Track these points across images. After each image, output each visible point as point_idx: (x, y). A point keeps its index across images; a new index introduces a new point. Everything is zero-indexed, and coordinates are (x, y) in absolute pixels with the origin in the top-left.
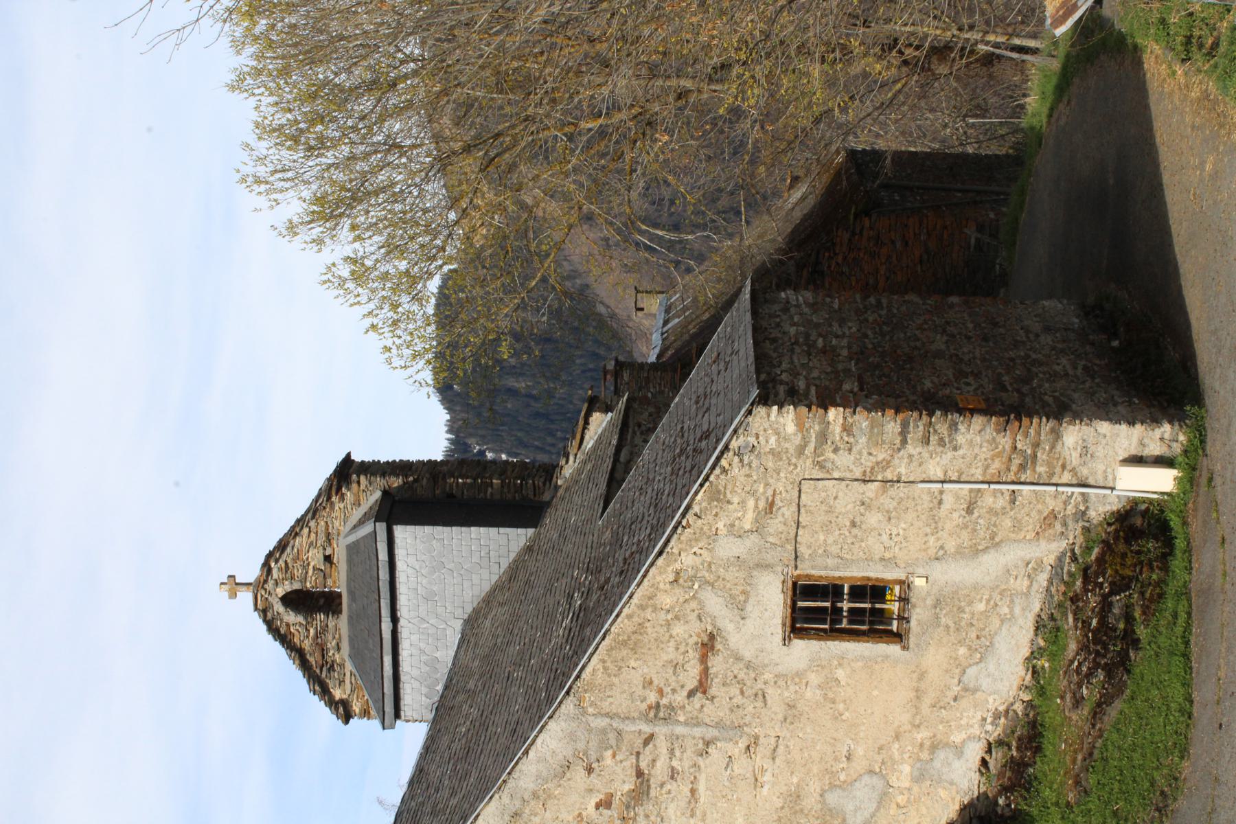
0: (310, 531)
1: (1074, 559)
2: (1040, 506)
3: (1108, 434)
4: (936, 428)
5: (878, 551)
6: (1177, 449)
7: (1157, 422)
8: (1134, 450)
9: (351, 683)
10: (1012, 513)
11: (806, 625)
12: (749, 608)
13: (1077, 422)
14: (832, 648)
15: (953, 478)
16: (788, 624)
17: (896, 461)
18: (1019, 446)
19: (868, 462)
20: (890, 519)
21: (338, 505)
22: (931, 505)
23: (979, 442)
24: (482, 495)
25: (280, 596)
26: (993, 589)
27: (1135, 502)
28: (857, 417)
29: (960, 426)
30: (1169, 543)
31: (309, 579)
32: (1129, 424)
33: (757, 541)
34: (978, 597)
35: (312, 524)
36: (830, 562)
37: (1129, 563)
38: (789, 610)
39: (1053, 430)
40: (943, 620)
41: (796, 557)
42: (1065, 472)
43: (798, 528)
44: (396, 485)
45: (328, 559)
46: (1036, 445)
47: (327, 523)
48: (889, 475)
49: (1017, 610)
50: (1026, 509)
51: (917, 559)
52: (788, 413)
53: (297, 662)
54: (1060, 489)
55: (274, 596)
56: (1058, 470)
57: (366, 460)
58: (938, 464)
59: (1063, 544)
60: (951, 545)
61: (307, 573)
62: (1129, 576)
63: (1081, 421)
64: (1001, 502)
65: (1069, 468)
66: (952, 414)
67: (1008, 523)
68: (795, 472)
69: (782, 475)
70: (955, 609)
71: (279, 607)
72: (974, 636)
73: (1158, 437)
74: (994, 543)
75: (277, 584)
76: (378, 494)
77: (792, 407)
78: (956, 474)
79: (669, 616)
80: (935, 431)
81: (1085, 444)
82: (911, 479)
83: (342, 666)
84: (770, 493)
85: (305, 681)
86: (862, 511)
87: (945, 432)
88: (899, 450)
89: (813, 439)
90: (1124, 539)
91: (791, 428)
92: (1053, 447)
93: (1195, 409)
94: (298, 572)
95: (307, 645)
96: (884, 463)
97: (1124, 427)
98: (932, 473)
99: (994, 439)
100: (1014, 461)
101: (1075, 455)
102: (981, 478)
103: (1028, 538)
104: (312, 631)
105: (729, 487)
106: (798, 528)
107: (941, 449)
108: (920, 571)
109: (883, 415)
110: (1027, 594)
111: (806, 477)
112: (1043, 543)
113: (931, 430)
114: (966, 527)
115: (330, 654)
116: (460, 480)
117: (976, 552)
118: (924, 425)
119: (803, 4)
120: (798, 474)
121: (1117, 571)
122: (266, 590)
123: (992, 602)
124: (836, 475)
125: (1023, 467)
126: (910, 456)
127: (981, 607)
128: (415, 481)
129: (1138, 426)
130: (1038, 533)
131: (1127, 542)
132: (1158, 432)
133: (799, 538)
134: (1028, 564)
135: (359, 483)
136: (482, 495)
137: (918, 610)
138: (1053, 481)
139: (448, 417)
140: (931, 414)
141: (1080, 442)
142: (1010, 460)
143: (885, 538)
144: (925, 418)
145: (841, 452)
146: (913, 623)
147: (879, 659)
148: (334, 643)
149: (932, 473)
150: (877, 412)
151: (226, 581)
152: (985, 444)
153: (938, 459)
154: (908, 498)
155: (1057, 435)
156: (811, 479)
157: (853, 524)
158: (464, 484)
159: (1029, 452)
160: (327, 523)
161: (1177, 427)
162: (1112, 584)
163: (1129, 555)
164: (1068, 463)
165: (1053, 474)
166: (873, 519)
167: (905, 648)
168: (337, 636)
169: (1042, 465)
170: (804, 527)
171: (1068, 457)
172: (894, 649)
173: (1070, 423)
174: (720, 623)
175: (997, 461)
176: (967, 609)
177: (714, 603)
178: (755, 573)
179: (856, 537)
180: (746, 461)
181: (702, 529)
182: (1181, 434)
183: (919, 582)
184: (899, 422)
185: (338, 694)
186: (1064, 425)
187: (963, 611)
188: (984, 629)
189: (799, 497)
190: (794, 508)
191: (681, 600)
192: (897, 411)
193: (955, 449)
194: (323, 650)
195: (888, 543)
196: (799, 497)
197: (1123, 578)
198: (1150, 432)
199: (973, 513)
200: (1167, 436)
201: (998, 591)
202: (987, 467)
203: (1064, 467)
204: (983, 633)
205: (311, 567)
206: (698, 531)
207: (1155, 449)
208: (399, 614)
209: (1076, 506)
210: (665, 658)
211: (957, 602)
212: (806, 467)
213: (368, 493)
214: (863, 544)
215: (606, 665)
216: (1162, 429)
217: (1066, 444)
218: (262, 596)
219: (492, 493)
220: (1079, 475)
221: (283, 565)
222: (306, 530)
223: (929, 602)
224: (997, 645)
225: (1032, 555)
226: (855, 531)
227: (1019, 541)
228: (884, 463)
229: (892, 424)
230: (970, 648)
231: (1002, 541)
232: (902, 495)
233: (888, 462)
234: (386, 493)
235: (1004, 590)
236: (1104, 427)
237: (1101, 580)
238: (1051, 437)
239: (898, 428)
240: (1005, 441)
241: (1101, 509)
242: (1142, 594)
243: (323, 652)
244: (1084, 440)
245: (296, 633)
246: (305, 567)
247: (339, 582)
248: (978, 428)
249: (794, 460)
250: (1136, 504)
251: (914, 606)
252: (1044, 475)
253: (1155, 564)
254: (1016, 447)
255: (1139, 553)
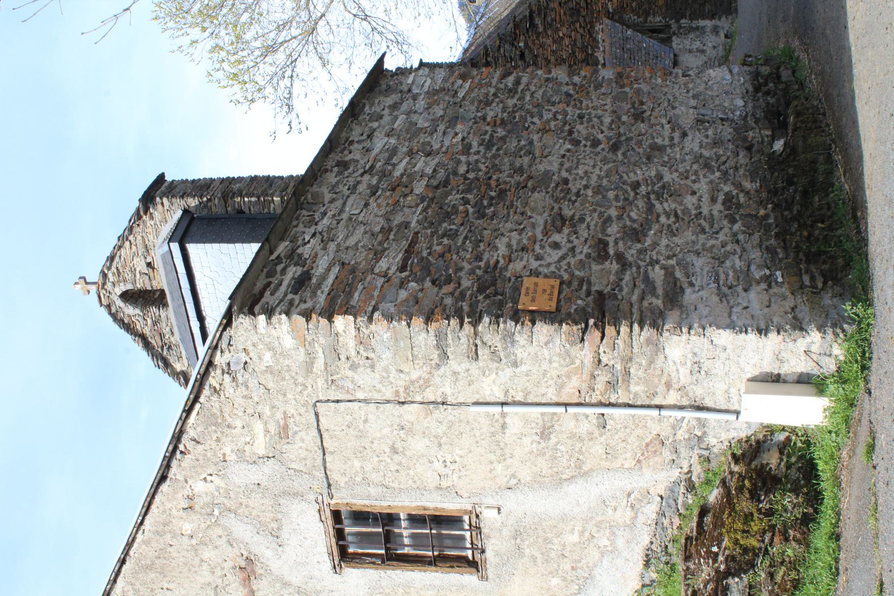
0: (131, 244)
1: (691, 487)
2: (639, 431)
3: (729, 346)
4: (485, 340)
5: (432, 480)
6: (830, 366)
7: (801, 329)
8: (769, 366)
10: (603, 439)
11: (360, 551)
12: (285, 534)
13: (685, 330)
14: (394, 576)
15: (517, 399)
16: (336, 553)
17: (437, 380)
18: (604, 360)
19: (401, 382)
20: (440, 445)
21: (149, 223)
22: (492, 430)
23: (548, 357)
24: (266, 210)
25: (119, 294)
26: (586, 521)
27: (771, 430)
28: (373, 327)
29: (517, 337)
30: (815, 498)
31: (138, 281)
32: (760, 331)
33: (277, 467)
34: (569, 528)
35: (131, 238)
36: (373, 491)
37: (755, 528)
38: (334, 540)
39: (649, 341)
40: (527, 551)
41: (329, 485)
42: (671, 392)
43: (324, 454)
44: (193, 204)
45: (149, 265)
46: (628, 359)
47: (143, 237)
48: (430, 396)
49: (620, 542)
50: (621, 435)
51: (484, 488)
52: (280, 323)
53: (141, 344)
54: (664, 413)
55: (113, 294)
56: (661, 388)
58: (494, 382)
59: (675, 474)
60: (525, 474)
62: (754, 549)
63: (690, 328)
64: (585, 427)
65: (676, 386)
66: (505, 322)
67: (599, 449)
68: (305, 393)
69: (289, 396)
70: (540, 540)
71: (119, 303)
72: (568, 567)
73: (803, 349)
74: (581, 473)
75: (114, 285)
76: (179, 213)
77: (284, 316)
78: (521, 394)
79: (194, 542)
80: (484, 344)
81: (696, 359)
82: (461, 400)
83: (177, 346)
84: (279, 416)
85: (150, 358)
86: (403, 436)
87: (499, 345)
88: (438, 366)
89: (321, 354)
90: (750, 492)
91: (288, 342)
92: (651, 362)
93: (859, 309)
94: (129, 276)
95: (147, 331)
96: (421, 382)
97: (752, 337)
98: (488, 392)
99: (568, 353)
100: (598, 379)
101: (684, 372)
102: (555, 399)
103: (626, 466)
104: (149, 321)
105: (227, 410)
106: (324, 454)
107: (496, 365)
108: (490, 501)
109: (409, 325)
110: (632, 526)
111: (321, 398)
112: (647, 473)
113: (478, 342)
114: (541, 454)
115: (167, 337)
116: (246, 199)
117: (559, 482)
118: (468, 336)
120: (309, 395)
121: (736, 542)
122: (106, 290)
123: (587, 534)
124: (360, 395)
125: (612, 385)
126: (455, 373)
127: (574, 538)
128: (209, 200)
129: (773, 336)
130: (639, 461)
131: (754, 496)
132: (802, 343)
133: (328, 465)
134: (629, 495)
135: (162, 203)
136: (266, 210)
137: (493, 541)
138: (657, 401)
140: (475, 324)
141: (690, 356)
142: (593, 377)
143: (438, 466)
144: (468, 328)
145: (361, 369)
146: (489, 554)
147: (454, 589)
148: (168, 329)
149: (488, 392)
150: (400, 319)
151: (78, 281)
152: (556, 358)
153: (493, 376)
154: (460, 421)
155: (658, 348)
156: (328, 401)
157: (394, 450)
158: (250, 202)
159: (618, 367)
160: (143, 237)
161: (830, 336)
162: (730, 559)
163: (756, 515)
164: (675, 381)
165: (655, 394)
166: (418, 445)
167: (483, 578)
168: (169, 324)
169: (637, 384)
170: (332, 453)
171: (673, 374)
172: (469, 579)
173: (672, 332)
174: (255, 549)
175: (574, 378)
176: (555, 541)
177: (243, 531)
178: (282, 501)
179: (400, 464)
180: (240, 380)
181: (205, 455)
182: (835, 346)
183: (488, 515)
184: (432, 332)
185: (178, 367)
186: (666, 334)
187: (551, 542)
188: (580, 562)
189: (318, 421)
190: (315, 433)
191: (203, 526)
192: (428, 320)
193: (515, 364)
194: (161, 334)
195: (443, 471)
196: (318, 421)
197: (745, 550)
198: (791, 344)
199: (549, 439)
200: (815, 348)
201: (594, 522)
202: (562, 386)
203: (668, 385)
204: (579, 565)
205: (137, 272)
206: (201, 458)
207: (797, 365)
208: (204, 314)
209: (689, 431)
210: (202, 581)
211: (541, 533)
212: (320, 388)
213: (172, 212)
214: (411, 472)
215: (135, 587)
216: (808, 339)
217: (670, 358)
218: (104, 295)
219: (274, 208)
220: (691, 394)
221: (115, 271)
222: (127, 243)
223: (506, 532)
224: (598, 577)
225: (635, 485)
226: (397, 458)
227: (616, 470)
228: (421, 382)
229: (424, 334)
230: (564, 579)
231: (592, 470)
232: (451, 418)
233: (427, 381)
234: (186, 212)
235: (601, 522)
236: (724, 337)
237: (715, 549)
238: (648, 350)
239: (432, 341)
240: (585, 354)
241: (725, 436)
242: (771, 575)
243: (161, 336)
244: (695, 354)
245: (137, 322)
247: (161, 281)
248: (543, 339)
249: (301, 380)
250: (772, 432)
251: (488, 537)
252: (643, 395)
253: (791, 533)
254: (600, 361)
255: (770, 513)
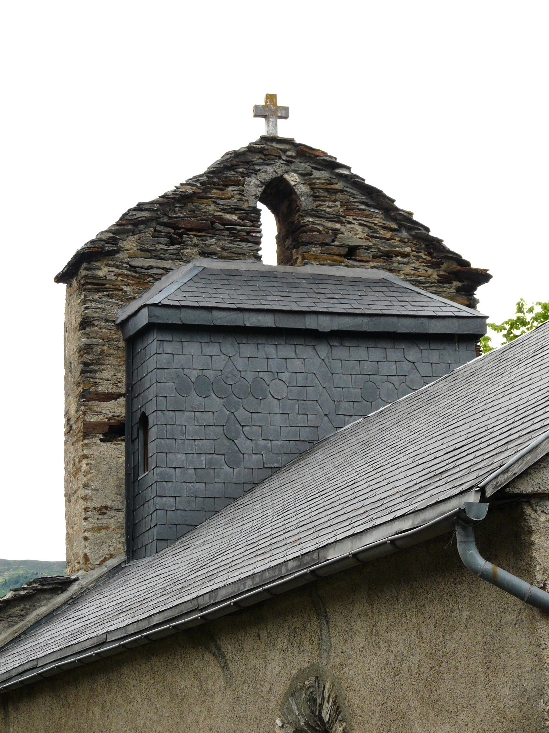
9: (151, 267)
55: (285, 168)
57: (276, 233)
61: (327, 219)
94: (327, 207)
119: (505, 336)
139: (431, 234)
168: (225, 254)
205: (338, 226)
218: (285, 151)
246: (337, 218)
